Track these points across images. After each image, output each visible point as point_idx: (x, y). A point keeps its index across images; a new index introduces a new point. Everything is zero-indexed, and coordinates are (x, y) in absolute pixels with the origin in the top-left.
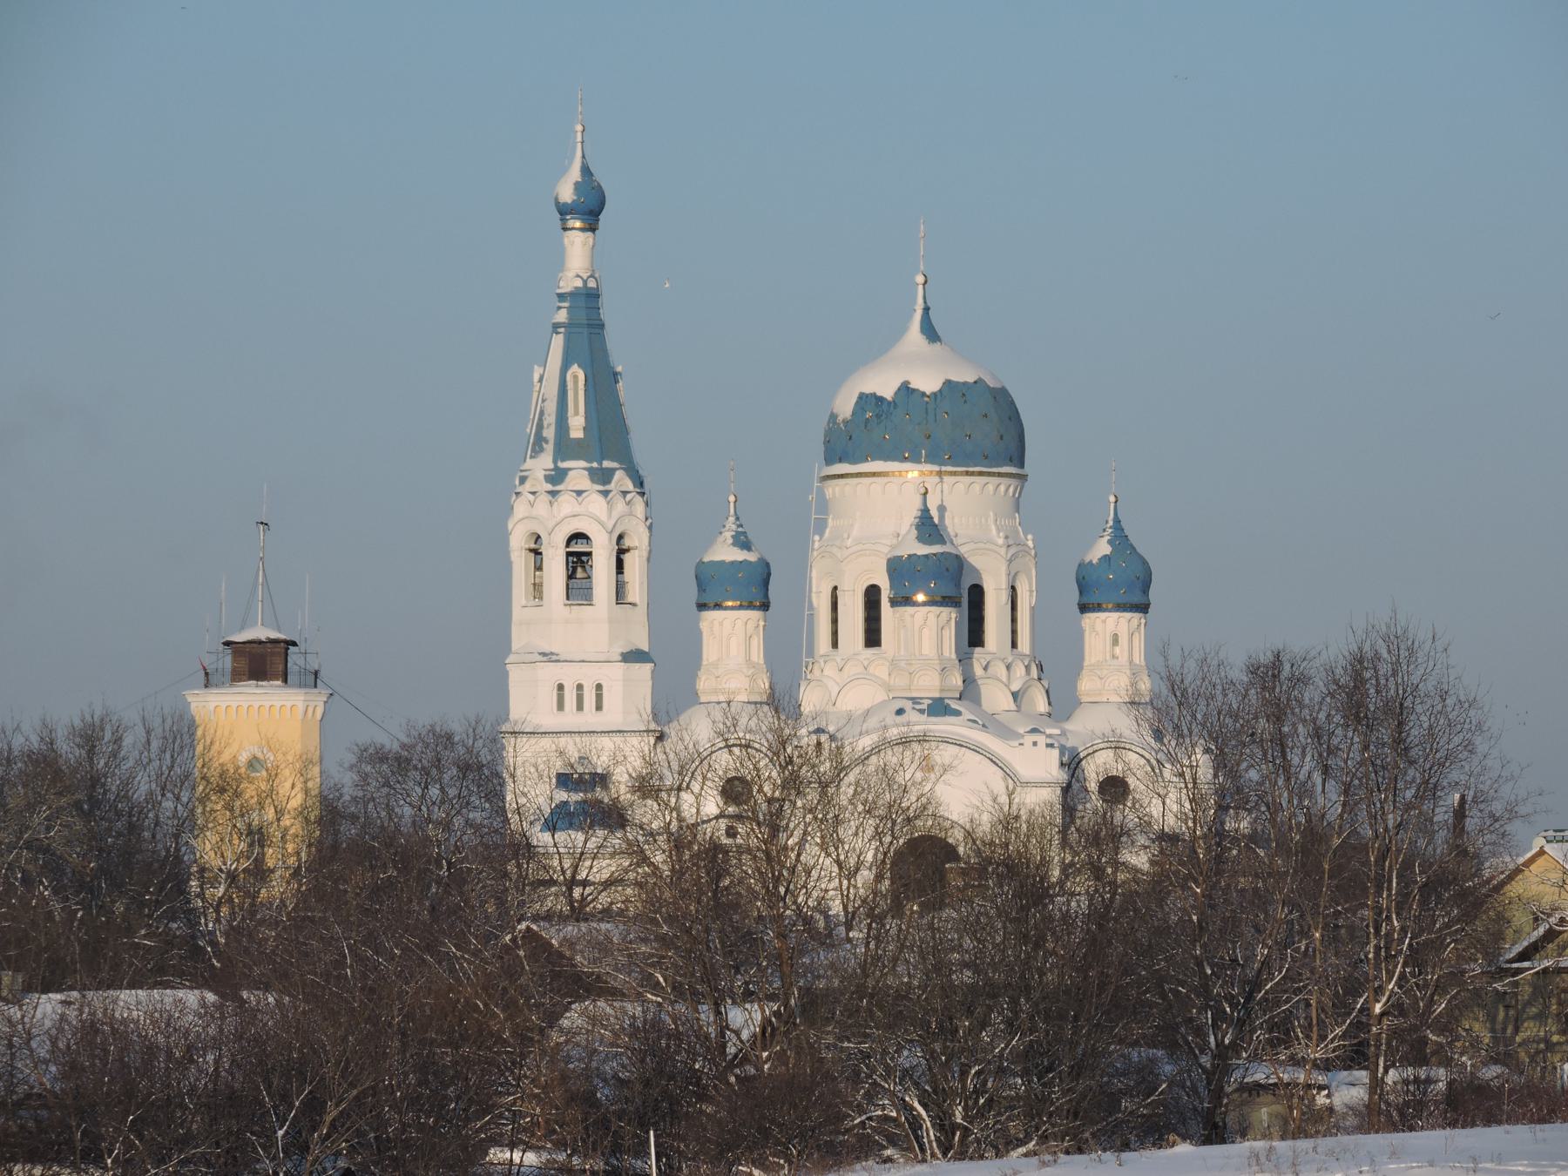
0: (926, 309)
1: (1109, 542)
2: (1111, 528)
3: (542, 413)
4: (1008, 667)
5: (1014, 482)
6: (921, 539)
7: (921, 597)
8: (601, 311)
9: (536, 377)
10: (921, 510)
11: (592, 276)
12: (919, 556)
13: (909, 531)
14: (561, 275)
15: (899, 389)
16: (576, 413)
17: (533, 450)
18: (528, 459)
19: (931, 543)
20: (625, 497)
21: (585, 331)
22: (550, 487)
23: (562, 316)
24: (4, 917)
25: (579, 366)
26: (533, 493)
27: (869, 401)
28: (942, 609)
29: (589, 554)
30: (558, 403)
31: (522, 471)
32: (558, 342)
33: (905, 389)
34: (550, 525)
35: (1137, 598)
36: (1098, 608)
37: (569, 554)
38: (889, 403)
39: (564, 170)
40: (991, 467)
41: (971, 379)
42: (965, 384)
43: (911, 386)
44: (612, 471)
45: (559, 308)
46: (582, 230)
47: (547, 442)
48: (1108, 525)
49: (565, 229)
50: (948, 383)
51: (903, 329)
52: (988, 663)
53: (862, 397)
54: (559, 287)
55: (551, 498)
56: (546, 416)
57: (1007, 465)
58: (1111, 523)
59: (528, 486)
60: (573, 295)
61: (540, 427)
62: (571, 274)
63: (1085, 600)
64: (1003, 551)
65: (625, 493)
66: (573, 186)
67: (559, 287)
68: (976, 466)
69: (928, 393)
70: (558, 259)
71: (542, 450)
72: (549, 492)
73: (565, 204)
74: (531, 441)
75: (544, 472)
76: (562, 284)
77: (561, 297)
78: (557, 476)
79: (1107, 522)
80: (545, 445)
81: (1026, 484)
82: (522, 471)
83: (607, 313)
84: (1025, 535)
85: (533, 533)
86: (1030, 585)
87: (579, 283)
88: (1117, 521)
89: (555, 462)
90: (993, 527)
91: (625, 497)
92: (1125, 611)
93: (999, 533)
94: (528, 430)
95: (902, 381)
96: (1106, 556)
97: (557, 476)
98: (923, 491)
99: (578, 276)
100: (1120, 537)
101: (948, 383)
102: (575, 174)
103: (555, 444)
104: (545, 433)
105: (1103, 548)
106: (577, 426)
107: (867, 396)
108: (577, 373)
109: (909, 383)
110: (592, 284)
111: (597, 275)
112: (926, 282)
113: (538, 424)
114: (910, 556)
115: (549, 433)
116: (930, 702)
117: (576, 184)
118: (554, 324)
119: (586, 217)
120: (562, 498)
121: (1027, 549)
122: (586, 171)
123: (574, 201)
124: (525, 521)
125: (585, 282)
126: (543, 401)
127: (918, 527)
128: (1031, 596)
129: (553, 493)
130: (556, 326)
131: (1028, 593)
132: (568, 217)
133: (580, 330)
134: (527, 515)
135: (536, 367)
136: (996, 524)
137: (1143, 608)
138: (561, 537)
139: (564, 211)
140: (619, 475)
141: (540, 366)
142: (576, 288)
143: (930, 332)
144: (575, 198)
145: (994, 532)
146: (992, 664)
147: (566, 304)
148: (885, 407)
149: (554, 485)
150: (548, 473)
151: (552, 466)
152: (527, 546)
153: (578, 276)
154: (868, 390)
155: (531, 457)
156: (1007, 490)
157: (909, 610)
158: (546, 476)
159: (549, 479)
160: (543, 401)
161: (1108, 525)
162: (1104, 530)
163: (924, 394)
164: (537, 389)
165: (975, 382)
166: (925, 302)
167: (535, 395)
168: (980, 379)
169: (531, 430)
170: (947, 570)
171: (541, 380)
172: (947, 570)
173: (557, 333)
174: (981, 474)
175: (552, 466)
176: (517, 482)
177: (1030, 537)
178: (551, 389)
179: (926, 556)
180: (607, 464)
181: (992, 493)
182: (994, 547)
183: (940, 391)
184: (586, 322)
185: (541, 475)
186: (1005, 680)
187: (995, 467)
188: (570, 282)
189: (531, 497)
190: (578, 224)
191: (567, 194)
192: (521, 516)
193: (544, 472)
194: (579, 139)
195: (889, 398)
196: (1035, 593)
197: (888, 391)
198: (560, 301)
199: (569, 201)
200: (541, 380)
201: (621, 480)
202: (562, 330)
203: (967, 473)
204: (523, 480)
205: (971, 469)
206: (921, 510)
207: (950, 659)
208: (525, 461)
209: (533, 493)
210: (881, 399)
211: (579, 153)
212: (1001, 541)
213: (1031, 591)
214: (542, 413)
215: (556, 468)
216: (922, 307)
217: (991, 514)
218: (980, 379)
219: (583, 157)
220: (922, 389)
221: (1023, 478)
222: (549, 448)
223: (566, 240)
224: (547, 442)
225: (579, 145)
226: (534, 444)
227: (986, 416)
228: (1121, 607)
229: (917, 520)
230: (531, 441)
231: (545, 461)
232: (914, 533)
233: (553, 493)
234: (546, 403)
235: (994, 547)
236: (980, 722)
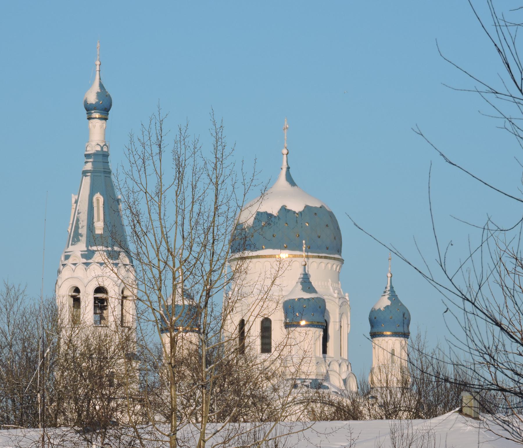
0: (288, 168)
1: (389, 298)
2: (389, 291)
3: (78, 220)
4: (340, 365)
5: (336, 263)
6: (304, 289)
7: (303, 323)
8: (110, 164)
9: (73, 201)
10: (303, 274)
11: (105, 145)
12: (305, 299)
13: (296, 286)
14: (87, 144)
15: (280, 209)
16: (99, 220)
17: (72, 241)
18: (70, 246)
19: (310, 292)
20: (125, 267)
21: (102, 175)
22: (85, 261)
23: (89, 167)
24: (267, 446)
25: (100, 194)
26: (75, 264)
27: (260, 216)
28: (316, 329)
29: (106, 300)
30: (88, 214)
31: (66, 252)
32: (87, 181)
33: (284, 210)
34: (86, 281)
35: (400, 330)
36: (381, 335)
37: (96, 299)
38: (275, 217)
39: (90, 86)
40: (331, 254)
41: (318, 206)
42: (316, 208)
43: (287, 208)
44: (119, 253)
45: (86, 162)
46: (99, 118)
47: (82, 236)
48: (387, 290)
49: (89, 119)
50: (307, 207)
51: (277, 179)
52: (330, 362)
53: (258, 214)
54: (86, 151)
55: (85, 267)
56: (80, 221)
57: (337, 254)
58: (389, 288)
59: (71, 261)
60: (96, 155)
61: (77, 227)
62: (94, 143)
63: (375, 330)
64: (337, 300)
65: (125, 265)
66: (96, 94)
67: (86, 151)
68: (323, 253)
69: (297, 212)
70: (87, 134)
71: (79, 240)
72: (84, 263)
73: (91, 104)
74: (72, 236)
75: (81, 253)
76: (88, 149)
77: (87, 156)
78: (88, 255)
79: (386, 288)
80: (80, 238)
81: (343, 265)
82: (66, 252)
83: (113, 164)
84: (344, 293)
85: (74, 287)
86: (348, 321)
87: (99, 149)
88: (392, 287)
89: (87, 246)
90: (331, 288)
91: (125, 267)
92: (399, 336)
93: (334, 292)
94: (69, 231)
95: (282, 205)
96: (388, 306)
97: (88, 255)
98: (304, 263)
99: (98, 144)
100: (393, 296)
101: (307, 207)
102: (96, 88)
103: (87, 237)
104: (80, 231)
105: (385, 302)
106: (99, 227)
107: (262, 213)
108: (99, 198)
109: (286, 207)
110: (105, 149)
111: (107, 145)
112: (288, 153)
113: (75, 227)
114: (299, 299)
115: (83, 231)
116: (311, 381)
117: (98, 93)
118: (83, 171)
119: (103, 112)
120: (92, 267)
121: (346, 300)
122: (101, 86)
123: (96, 103)
124: (69, 280)
125: (102, 148)
126: (79, 213)
127: (302, 283)
128: (348, 327)
129: (87, 264)
130: (85, 173)
131: (347, 325)
132: (93, 112)
133: (99, 174)
134: (70, 276)
135: (73, 195)
136: (332, 286)
137: (406, 335)
138: (91, 289)
139: (89, 108)
140: (122, 255)
141: (75, 194)
142: (97, 151)
143: (290, 179)
144: (97, 101)
145: (332, 290)
146: (332, 363)
147: (91, 160)
148: (273, 219)
149: (87, 259)
150: (83, 253)
151: (86, 249)
152: (70, 294)
153: (98, 144)
154: (262, 209)
155: (72, 245)
156: (336, 268)
157: (298, 329)
158: (82, 255)
159: (83, 256)
160: (79, 213)
161: (387, 290)
162: (385, 292)
163: (294, 212)
164: (75, 207)
165: (321, 207)
166: (287, 164)
167: (73, 211)
168: (322, 206)
169: (70, 229)
170: (320, 307)
171: (76, 202)
172: (320, 307)
173: (86, 176)
174: (326, 258)
175: (86, 249)
176: (63, 259)
177: (347, 294)
178: (83, 206)
179: (308, 299)
180: (116, 248)
181: (324, 268)
182: (332, 298)
183: (303, 211)
184: (103, 170)
185: (79, 254)
186: (338, 371)
187: (333, 254)
188: (93, 148)
189: (73, 267)
190: (97, 115)
191: (92, 98)
192: (67, 277)
193: (81, 253)
194: (98, 69)
195: (275, 215)
196: (349, 326)
197: (274, 210)
198: (87, 159)
199: (94, 103)
200: (76, 202)
201: (124, 259)
202: (89, 174)
203: (319, 257)
204: (67, 257)
205: (321, 255)
206: (303, 274)
207: (320, 358)
208: (68, 247)
209: (75, 264)
210: (271, 215)
211: (97, 77)
212: (336, 295)
213: (348, 324)
214: (78, 220)
215: (88, 250)
216: (286, 167)
217: (330, 280)
218: (322, 206)
219: (100, 79)
220: (293, 209)
221: (342, 261)
222: (84, 239)
223: (90, 125)
224: (82, 236)
225: (98, 72)
226: (73, 237)
227: (327, 226)
228: (396, 334)
229: (301, 280)
230: (72, 236)
231: (82, 246)
232: (300, 286)
233: (87, 264)
234: (80, 215)
235: (332, 298)
236: (340, 393)
